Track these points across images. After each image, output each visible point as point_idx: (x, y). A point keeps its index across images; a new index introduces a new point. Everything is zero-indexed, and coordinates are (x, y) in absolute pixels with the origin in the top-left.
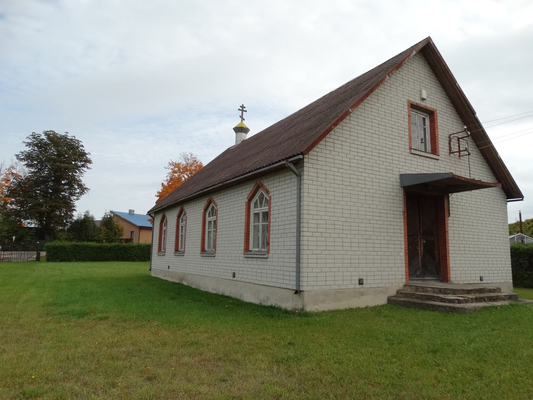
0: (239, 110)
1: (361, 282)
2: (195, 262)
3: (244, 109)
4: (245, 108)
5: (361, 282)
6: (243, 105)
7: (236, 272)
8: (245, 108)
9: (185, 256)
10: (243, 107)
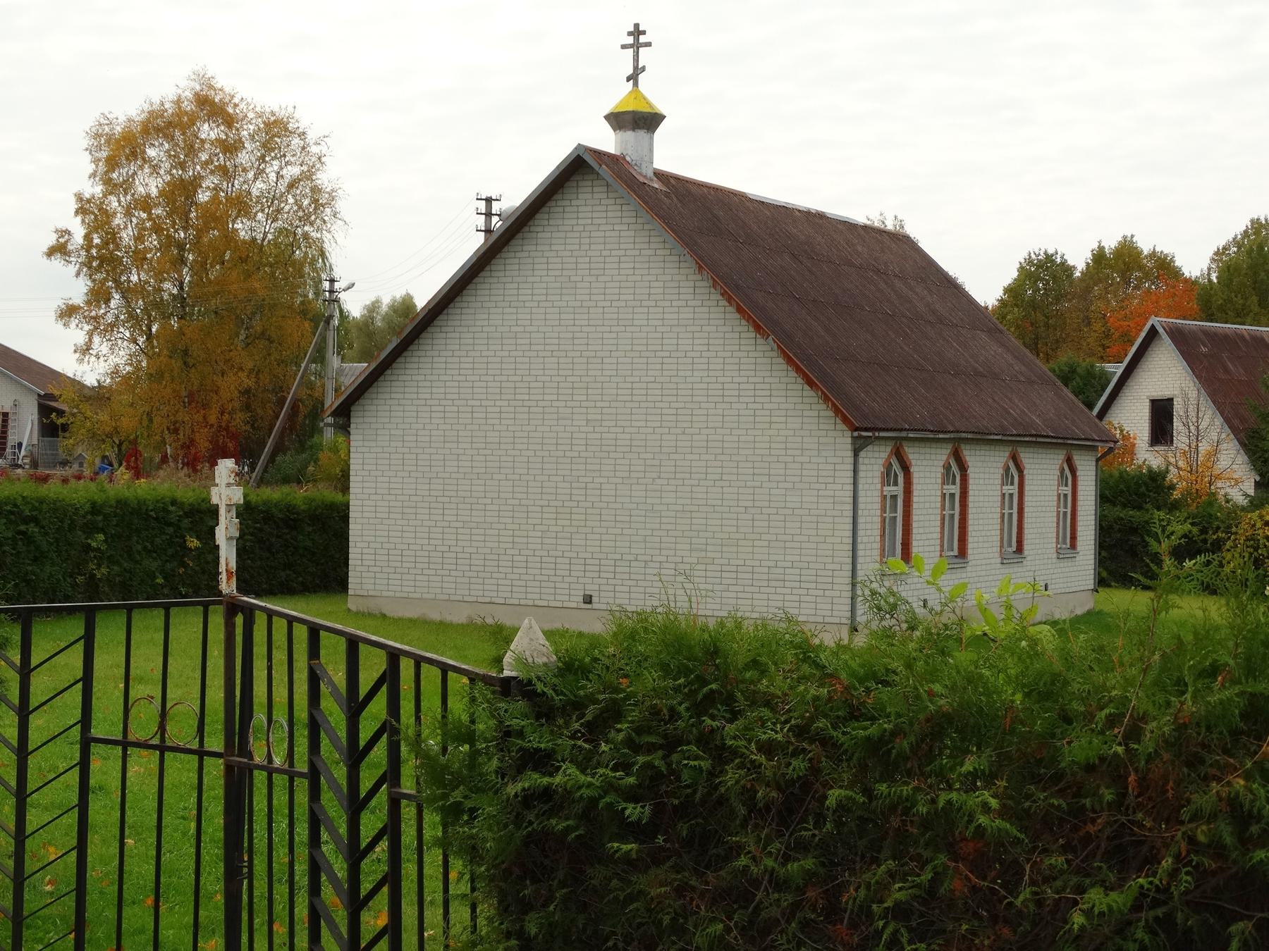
0: (624, 47)
1: (588, 600)
2: (991, 578)
3: (642, 39)
4: (644, 33)
5: (588, 600)
6: (637, 26)
7: (1049, 582)
8: (644, 33)
9: (969, 569)
10: (637, 32)
